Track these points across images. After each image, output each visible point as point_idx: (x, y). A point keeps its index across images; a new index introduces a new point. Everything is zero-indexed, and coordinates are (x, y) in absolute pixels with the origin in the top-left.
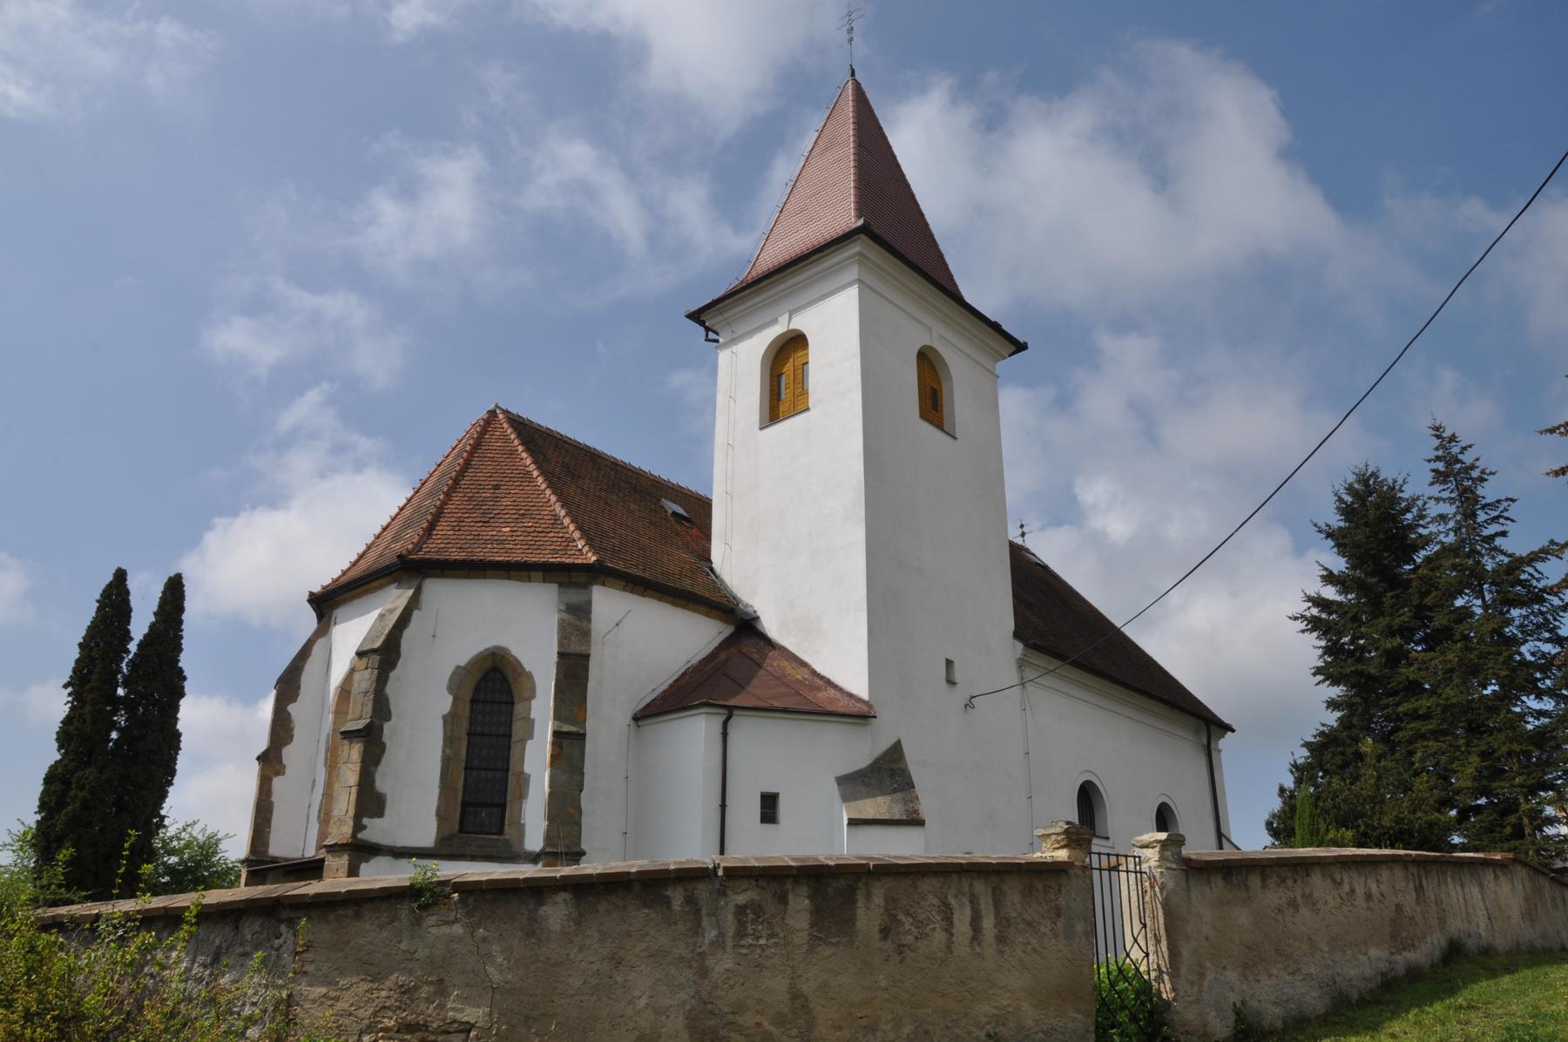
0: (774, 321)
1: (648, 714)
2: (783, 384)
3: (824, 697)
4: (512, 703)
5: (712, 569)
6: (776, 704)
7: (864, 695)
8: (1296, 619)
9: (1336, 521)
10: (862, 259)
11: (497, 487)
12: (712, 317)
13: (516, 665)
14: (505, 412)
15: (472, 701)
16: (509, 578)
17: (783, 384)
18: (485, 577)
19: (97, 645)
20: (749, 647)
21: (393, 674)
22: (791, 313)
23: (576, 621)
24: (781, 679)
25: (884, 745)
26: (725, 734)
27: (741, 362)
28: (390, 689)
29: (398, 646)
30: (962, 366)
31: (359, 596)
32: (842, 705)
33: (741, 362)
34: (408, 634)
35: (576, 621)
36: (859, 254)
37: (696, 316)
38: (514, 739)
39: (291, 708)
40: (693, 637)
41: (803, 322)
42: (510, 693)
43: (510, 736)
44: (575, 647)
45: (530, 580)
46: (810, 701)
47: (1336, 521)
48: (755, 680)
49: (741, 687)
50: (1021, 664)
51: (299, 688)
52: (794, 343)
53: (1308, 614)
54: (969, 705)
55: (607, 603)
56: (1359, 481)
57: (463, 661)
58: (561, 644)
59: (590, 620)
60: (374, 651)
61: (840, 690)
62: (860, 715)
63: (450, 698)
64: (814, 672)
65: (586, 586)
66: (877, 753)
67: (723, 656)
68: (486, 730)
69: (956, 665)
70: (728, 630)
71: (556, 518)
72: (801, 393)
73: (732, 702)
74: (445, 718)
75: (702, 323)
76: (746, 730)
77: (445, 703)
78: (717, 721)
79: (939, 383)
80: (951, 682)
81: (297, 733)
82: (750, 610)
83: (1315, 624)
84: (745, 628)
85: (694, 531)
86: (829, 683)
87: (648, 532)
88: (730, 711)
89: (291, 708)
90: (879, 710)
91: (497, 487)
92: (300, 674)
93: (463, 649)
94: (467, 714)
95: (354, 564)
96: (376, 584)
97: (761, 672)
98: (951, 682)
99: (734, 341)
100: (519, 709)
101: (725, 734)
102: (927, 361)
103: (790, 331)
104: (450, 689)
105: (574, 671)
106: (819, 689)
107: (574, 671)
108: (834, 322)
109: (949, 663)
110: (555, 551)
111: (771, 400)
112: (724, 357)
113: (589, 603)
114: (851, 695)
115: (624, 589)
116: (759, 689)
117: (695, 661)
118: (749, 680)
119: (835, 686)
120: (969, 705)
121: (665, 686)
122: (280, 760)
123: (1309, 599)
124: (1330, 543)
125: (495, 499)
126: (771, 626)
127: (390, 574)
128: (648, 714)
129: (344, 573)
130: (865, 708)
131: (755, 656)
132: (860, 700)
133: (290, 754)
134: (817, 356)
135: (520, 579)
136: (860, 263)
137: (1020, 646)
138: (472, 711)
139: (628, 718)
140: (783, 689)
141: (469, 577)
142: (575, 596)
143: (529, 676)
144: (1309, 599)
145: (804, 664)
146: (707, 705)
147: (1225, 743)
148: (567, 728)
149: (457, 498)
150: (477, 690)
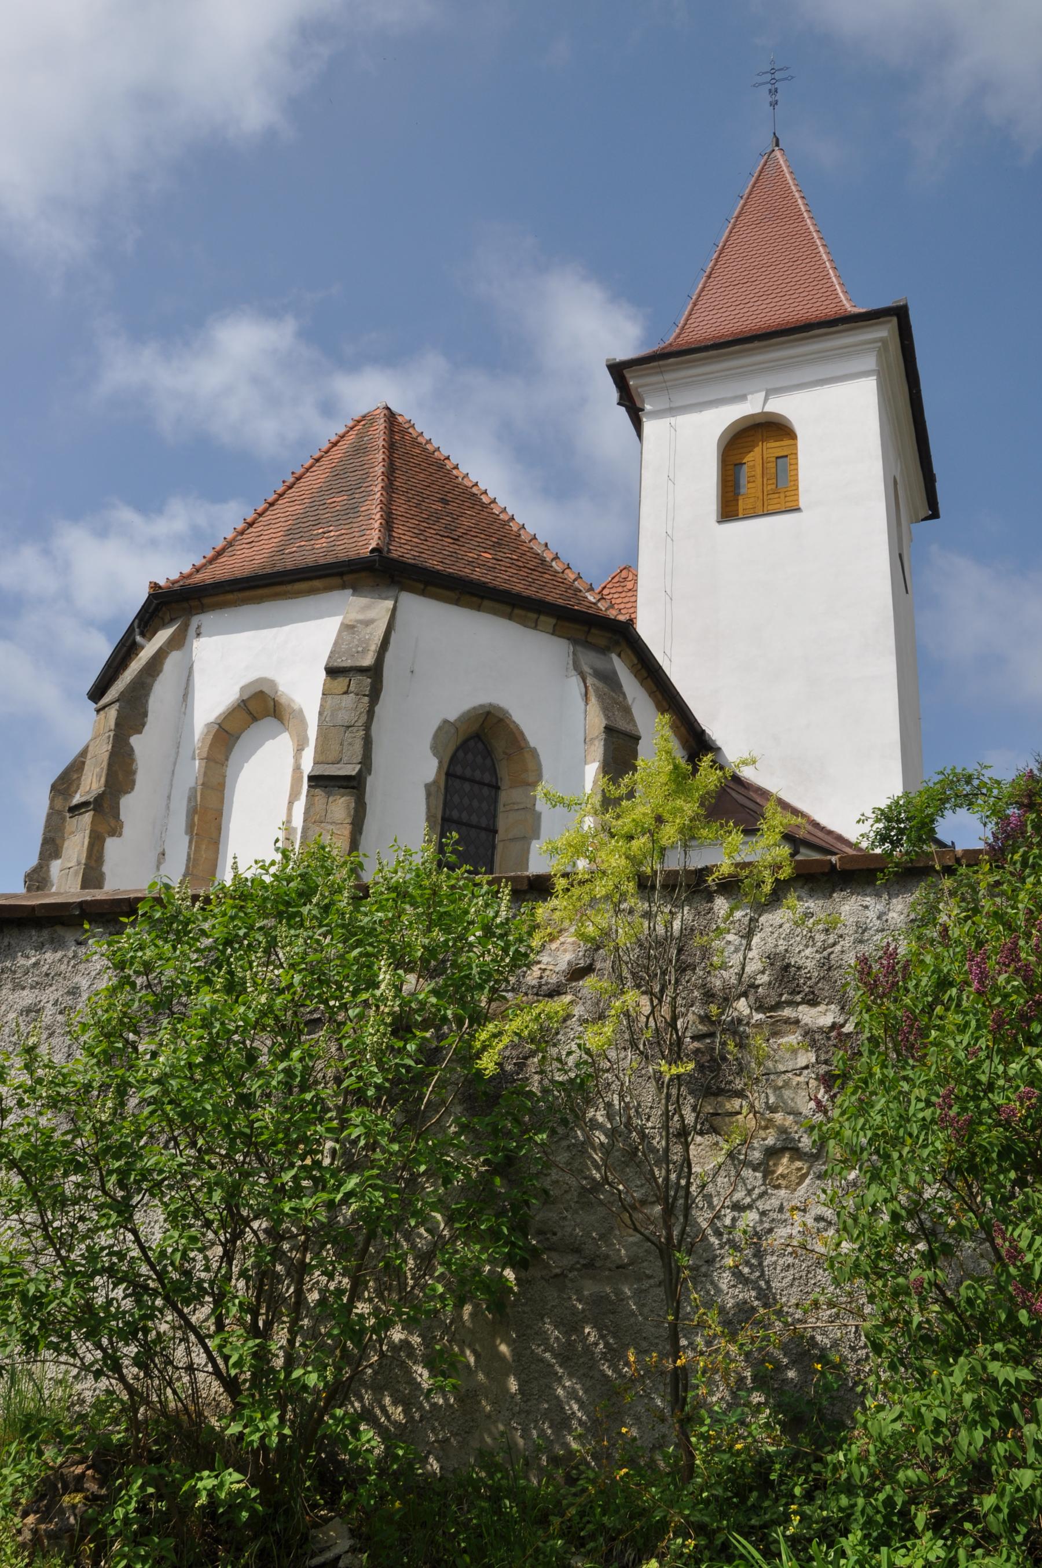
0: (743, 398)
2: (754, 469)
13: (516, 740)
16: (510, 617)
17: (754, 469)
18: (479, 608)
19: (166, 988)
22: (769, 393)
27: (686, 440)
29: (162, 664)
31: (260, 600)
33: (686, 440)
36: (883, 340)
38: (498, 837)
39: (135, 741)
45: (535, 628)
51: (145, 714)
68: (465, 817)
81: (140, 778)
89: (135, 741)
92: (147, 695)
93: (455, 702)
95: (198, 570)
96: (299, 586)
99: (672, 411)
103: (763, 414)
122: (116, 815)
127: (341, 574)
129: (183, 577)
133: (131, 806)
135: (523, 622)
141: (457, 602)
143: (534, 753)
149: (400, 500)
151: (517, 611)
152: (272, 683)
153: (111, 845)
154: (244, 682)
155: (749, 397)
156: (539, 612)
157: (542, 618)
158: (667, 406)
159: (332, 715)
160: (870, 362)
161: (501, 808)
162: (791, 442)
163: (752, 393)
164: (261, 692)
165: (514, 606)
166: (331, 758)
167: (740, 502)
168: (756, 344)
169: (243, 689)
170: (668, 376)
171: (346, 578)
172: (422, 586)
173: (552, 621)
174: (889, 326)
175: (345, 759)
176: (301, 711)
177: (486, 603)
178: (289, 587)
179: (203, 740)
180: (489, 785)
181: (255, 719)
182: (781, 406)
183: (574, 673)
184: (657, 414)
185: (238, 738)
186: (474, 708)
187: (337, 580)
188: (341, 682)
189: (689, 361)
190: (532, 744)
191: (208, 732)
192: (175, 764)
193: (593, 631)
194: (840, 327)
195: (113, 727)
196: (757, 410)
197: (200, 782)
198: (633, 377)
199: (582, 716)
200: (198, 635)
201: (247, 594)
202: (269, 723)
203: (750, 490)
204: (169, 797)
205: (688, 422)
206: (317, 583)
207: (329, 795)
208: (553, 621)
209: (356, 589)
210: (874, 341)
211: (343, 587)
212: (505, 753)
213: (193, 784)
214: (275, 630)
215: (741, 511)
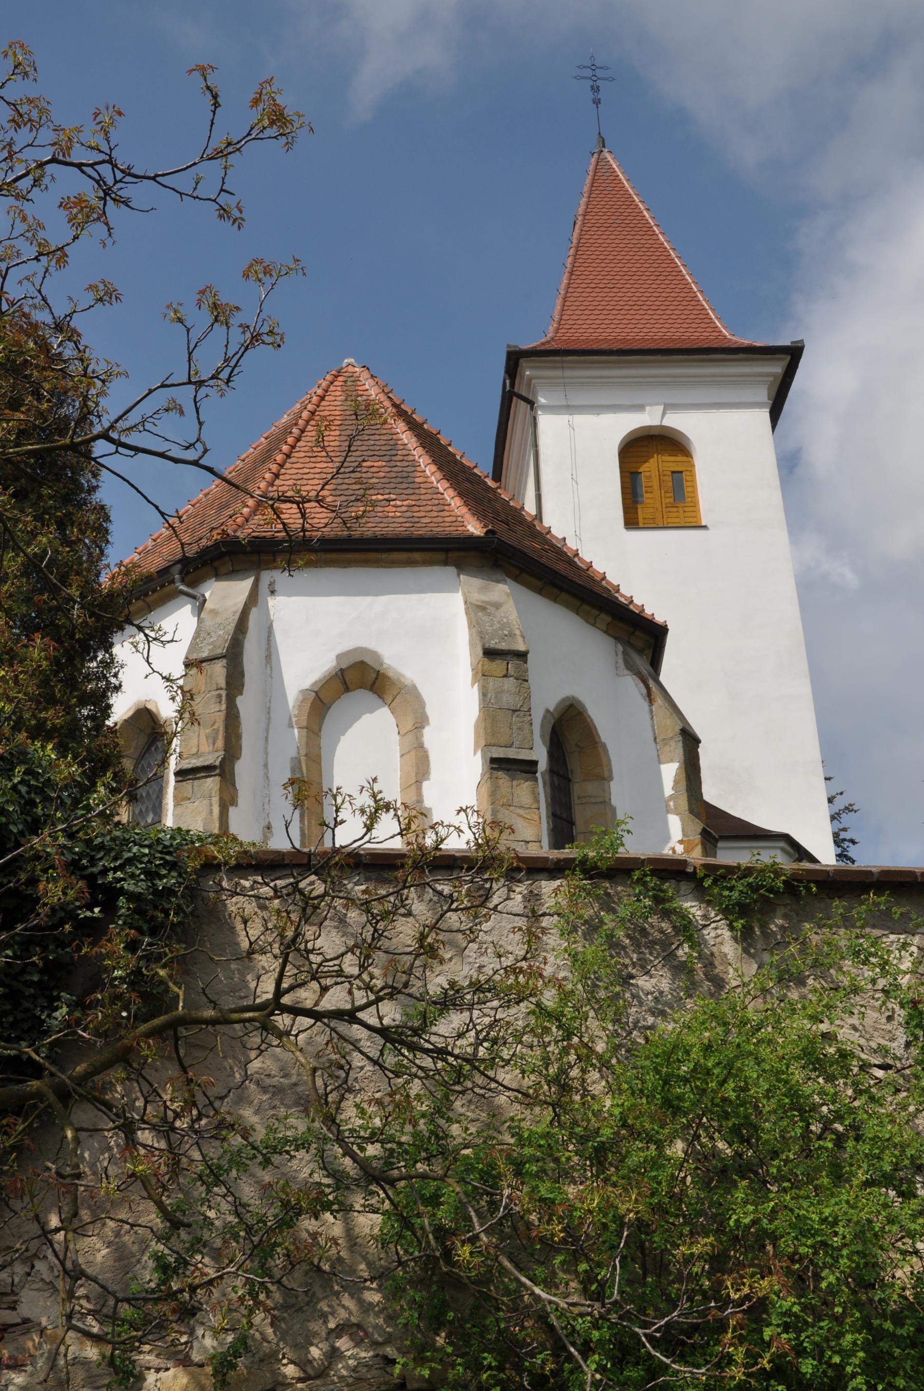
0: (640, 408)
18: (555, 599)
22: (669, 407)
36: (774, 375)
99: (569, 409)
127: (447, 551)
133: (244, 770)
141: (539, 591)
143: (604, 746)
151: (585, 607)
152: (375, 655)
153: (232, 811)
154: (340, 650)
155: (648, 408)
156: (601, 609)
157: (603, 616)
158: (564, 403)
159: (496, 697)
161: (575, 801)
162: (685, 459)
163: (651, 405)
164: (362, 662)
165: (583, 601)
166: (502, 741)
167: (640, 511)
168: (659, 357)
169: (339, 657)
170: (568, 373)
171: (450, 555)
172: (517, 572)
175: (516, 744)
176: (414, 687)
177: (564, 596)
178: (384, 556)
179: (300, 707)
181: (347, 689)
182: (678, 421)
183: (626, 672)
184: (552, 409)
185: (329, 708)
187: (441, 556)
188: (498, 666)
189: (593, 362)
190: (603, 739)
191: (304, 700)
192: (267, 730)
193: (637, 633)
194: (741, 356)
195: (223, 684)
196: (655, 422)
197: (303, 752)
198: (531, 368)
199: (648, 716)
200: (273, 592)
201: (334, 556)
202: (362, 696)
203: (653, 498)
204: (266, 766)
205: (584, 422)
206: (417, 556)
207: (513, 778)
208: (609, 619)
209: (461, 567)
211: (446, 563)
212: (577, 746)
213: (294, 753)
214: (369, 599)
215: (641, 520)
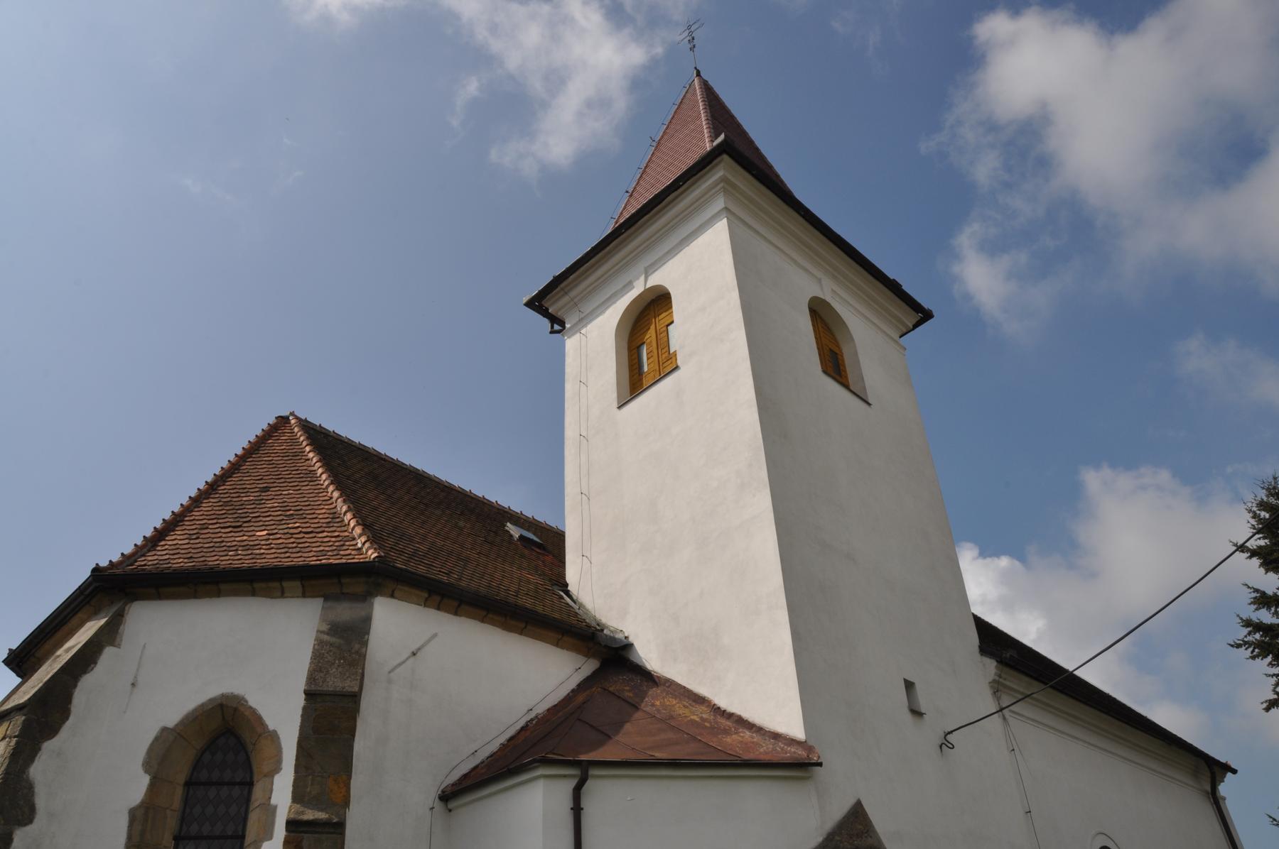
0: (629, 286)
1: (461, 791)
3: (735, 742)
4: (250, 784)
5: (568, 593)
6: (659, 755)
7: (798, 732)
8: (1239, 646)
9: (1259, 542)
10: (728, 187)
11: (266, 489)
12: (552, 303)
14: (306, 426)
15: (188, 784)
16: (254, 593)
17: (644, 350)
18: (218, 594)
20: (620, 684)
21: (48, 746)
23: (344, 649)
24: (668, 722)
25: (838, 810)
26: (577, 810)
27: (593, 344)
28: (38, 771)
29: (68, 699)
30: (865, 332)
32: (765, 750)
33: (593, 344)
34: (88, 683)
35: (344, 649)
36: (724, 180)
37: (537, 303)
40: (540, 676)
41: (666, 276)
42: (248, 766)
43: (243, 837)
44: (335, 682)
45: (282, 595)
46: (718, 751)
47: (1259, 542)
48: (628, 726)
49: (605, 737)
50: (997, 688)
52: (658, 302)
53: (1250, 638)
54: (945, 744)
55: (394, 623)
56: (1270, 494)
57: (172, 718)
58: (311, 679)
59: (365, 644)
60: (19, 708)
61: (759, 730)
62: (795, 765)
63: (145, 780)
64: (717, 710)
65: (366, 597)
66: (829, 825)
67: (581, 698)
69: (918, 687)
70: (589, 667)
71: (335, 516)
72: (667, 365)
73: (583, 758)
74: (133, 813)
75: (544, 312)
76: (611, 798)
77: (137, 787)
78: (564, 789)
79: (838, 346)
80: (916, 713)
82: (619, 636)
83: (1262, 649)
84: (612, 658)
85: (549, 559)
86: (741, 722)
87: (496, 564)
88: (584, 772)
90: (824, 753)
91: (266, 489)
94: (177, 802)
97: (638, 715)
98: (916, 713)
100: (258, 792)
101: (577, 810)
102: (820, 314)
104: (147, 766)
105: (332, 715)
106: (726, 732)
107: (332, 715)
108: (702, 269)
109: (909, 685)
110: (323, 553)
111: (631, 376)
112: (572, 344)
113: (367, 620)
114: (776, 736)
115: (426, 604)
116: (632, 738)
117: (541, 709)
118: (618, 726)
119: (750, 726)
120: (945, 744)
121: (494, 747)
123: (1247, 623)
124: (1256, 561)
125: (259, 502)
126: (649, 655)
128: (461, 791)
130: (801, 753)
131: (628, 695)
132: (793, 742)
134: (683, 330)
135: (269, 594)
136: (725, 191)
137: (991, 665)
138: (186, 800)
139: (434, 793)
140: (670, 735)
142: (346, 612)
144: (1247, 623)
145: (700, 700)
146: (546, 762)
147: (1226, 788)
148: (310, 815)
150: (197, 765)
151: (256, 585)
156: (281, 580)
157: (285, 584)
160: (719, 203)
173: (297, 584)
174: (722, 165)
177: (223, 587)
180: (241, 784)
182: (655, 280)
186: (202, 705)
190: (271, 727)
193: (343, 581)
196: (642, 289)
210: (716, 184)
